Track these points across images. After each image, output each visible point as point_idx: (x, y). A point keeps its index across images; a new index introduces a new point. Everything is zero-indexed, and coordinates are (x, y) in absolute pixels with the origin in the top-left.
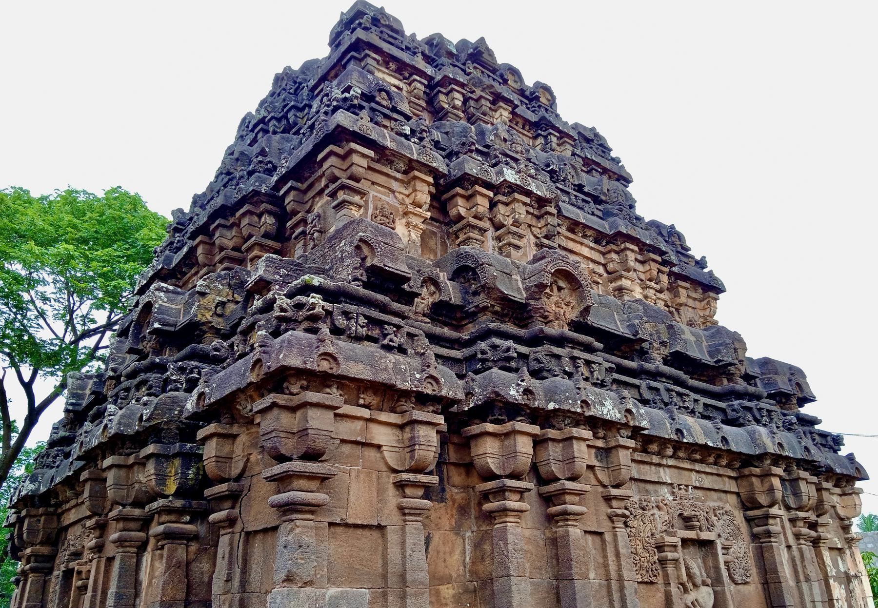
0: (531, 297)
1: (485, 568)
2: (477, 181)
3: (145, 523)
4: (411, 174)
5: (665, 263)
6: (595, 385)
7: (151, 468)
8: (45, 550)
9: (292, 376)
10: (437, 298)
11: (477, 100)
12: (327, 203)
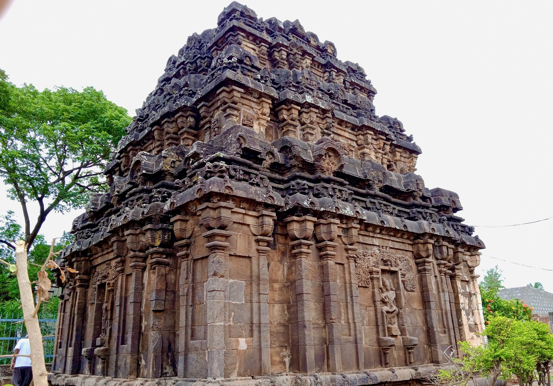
0: (316, 160)
1: (292, 277)
2: (292, 102)
3: (145, 259)
4: (261, 99)
5: (388, 140)
6: (343, 200)
7: (148, 234)
8: (85, 277)
9: (214, 195)
10: (273, 161)
11: (294, 55)
12: (221, 114)
